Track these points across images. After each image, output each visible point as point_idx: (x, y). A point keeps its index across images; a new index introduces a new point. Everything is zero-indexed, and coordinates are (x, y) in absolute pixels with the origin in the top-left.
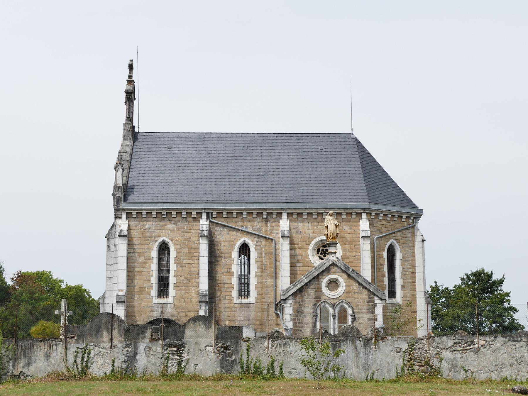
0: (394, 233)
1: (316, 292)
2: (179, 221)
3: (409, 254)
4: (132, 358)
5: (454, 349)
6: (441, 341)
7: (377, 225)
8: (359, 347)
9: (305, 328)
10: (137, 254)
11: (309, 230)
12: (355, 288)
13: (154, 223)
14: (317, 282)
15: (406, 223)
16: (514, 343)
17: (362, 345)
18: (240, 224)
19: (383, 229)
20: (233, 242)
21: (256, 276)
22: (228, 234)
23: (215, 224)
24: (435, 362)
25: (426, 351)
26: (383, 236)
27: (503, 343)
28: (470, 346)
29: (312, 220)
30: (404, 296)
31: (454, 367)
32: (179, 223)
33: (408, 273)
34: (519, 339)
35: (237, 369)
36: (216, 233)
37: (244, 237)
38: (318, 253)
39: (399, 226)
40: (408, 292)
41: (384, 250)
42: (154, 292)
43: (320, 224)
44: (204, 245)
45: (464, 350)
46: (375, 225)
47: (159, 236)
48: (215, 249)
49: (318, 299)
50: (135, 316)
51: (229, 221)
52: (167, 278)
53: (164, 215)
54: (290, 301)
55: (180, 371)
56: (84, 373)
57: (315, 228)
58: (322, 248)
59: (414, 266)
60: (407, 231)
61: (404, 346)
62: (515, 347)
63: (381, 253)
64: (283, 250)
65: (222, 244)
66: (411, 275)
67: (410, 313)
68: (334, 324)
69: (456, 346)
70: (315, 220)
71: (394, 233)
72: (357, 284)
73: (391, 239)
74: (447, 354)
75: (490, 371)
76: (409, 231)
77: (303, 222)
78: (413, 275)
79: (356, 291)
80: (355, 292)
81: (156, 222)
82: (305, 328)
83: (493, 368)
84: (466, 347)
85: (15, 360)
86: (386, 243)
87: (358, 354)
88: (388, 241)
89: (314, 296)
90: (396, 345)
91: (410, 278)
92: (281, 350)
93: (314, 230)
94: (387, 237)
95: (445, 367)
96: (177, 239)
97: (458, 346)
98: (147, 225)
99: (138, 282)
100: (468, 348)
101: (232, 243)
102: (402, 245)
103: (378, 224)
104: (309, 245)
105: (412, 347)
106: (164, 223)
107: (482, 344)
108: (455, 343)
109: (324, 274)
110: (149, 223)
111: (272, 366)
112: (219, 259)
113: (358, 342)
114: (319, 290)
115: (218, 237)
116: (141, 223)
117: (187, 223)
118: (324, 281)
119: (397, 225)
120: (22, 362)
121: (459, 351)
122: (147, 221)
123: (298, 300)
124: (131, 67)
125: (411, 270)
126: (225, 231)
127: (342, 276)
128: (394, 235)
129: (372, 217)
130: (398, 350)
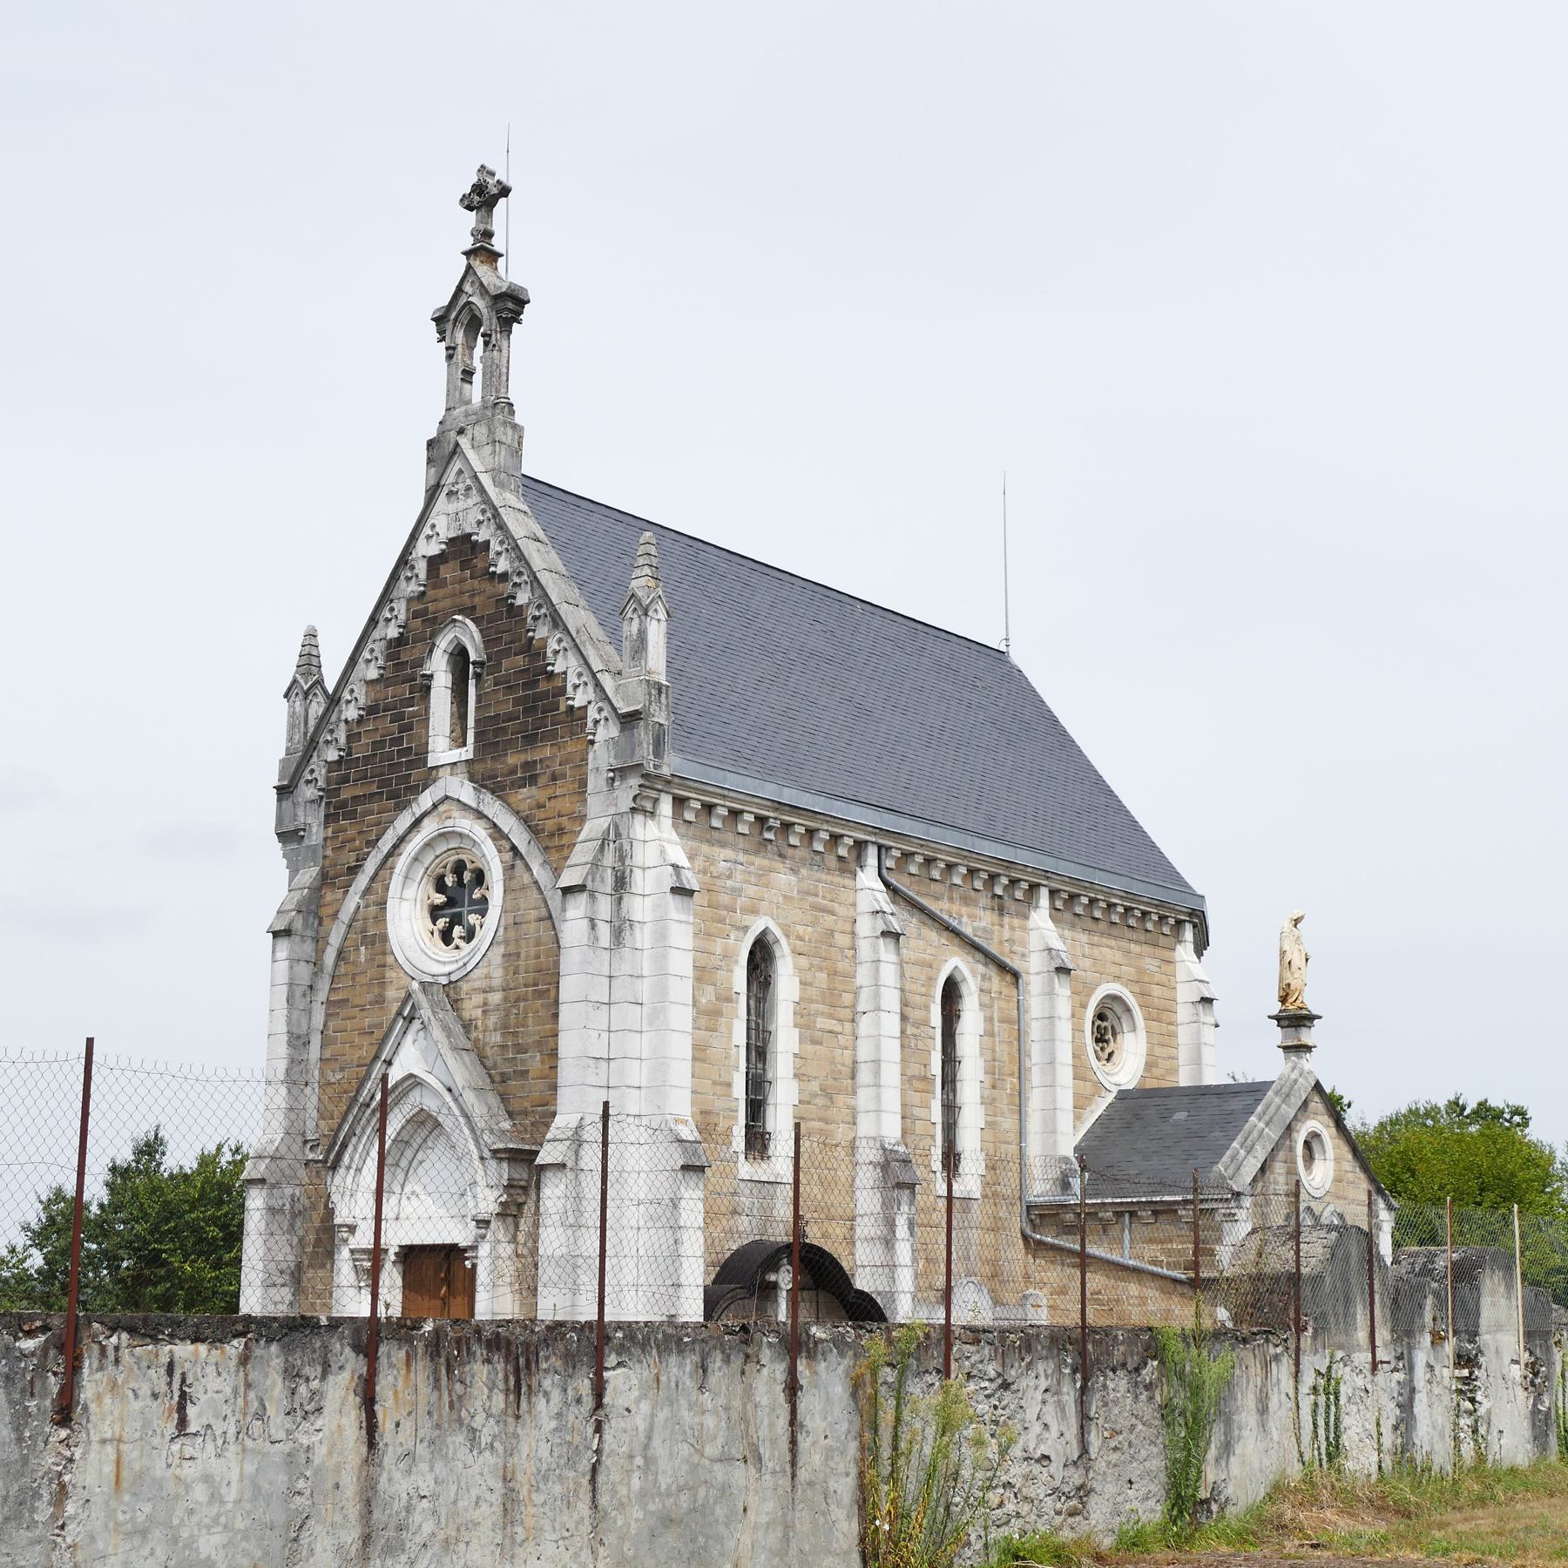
2: (803, 861)
13: (741, 857)
32: (804, 872)
43: (1104, 940)
47: (754, 911)
81: (746, 852)
96: (801, 929)
106: (766, 862)
117: (824, 876)
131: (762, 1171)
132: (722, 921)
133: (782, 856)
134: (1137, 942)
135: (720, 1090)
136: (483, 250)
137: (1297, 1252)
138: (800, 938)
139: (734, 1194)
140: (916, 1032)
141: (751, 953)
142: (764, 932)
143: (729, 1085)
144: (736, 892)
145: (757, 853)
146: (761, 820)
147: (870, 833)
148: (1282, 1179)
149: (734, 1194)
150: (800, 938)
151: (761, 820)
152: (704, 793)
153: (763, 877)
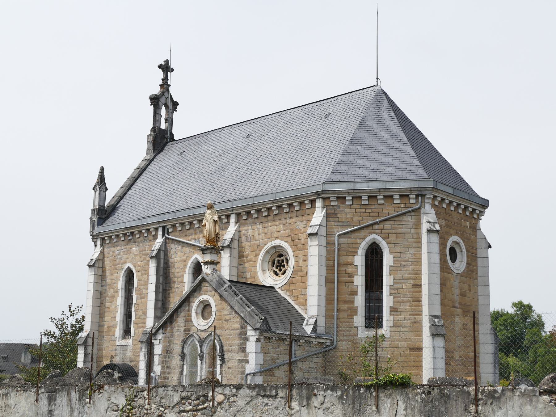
0: (376, 223)
1: (186, 321)
2: (141, 241)
3: (410, 255)
5: (182, 409)
6: (166, 394)
7: (344, 215)
8: (74, 400)
9: (173, 375)
10: (108, 286)
11: (259, 234)
12: (226, 313)
13: (123, 248)
14: (187, 308)
15: (402, 206)
16: (266, 400)
17: (78, 398)
18: (193, 237)
19: (354, 219)
20: (185, 261)
21: (297, 304)
22: (182, 251)
23: (171, 241)
25: (147, 410)
26: (352, 231)
27: (248, 399)
28: (204, 403)
29: (263, 219)
30: (396, 325)
32: (141, 245)
33: (406, 287)
34: (274, 393)
36: (172, 252)
37: (196, 253)
38: (273, 266)
40: (404, 317)
41: (356, 252)
42: (359, 320)
43: (271, 224)
46: (339, 215)
47: (125, 263)
48: (169, 273)
49: (187, 330)
50: (102, 361)
51: (184, 234)
52: (131, 313)
53: (129, 236)
54: (160, 337)
57: (266, 230)
58: (277, 259)
59: (418, 275)
60: (405, 218)
62: (266, 408)
63: (350, 258)
64: (223, 266)
65: (176, 265)
66: (412, 290)
67: (408, 352)
68: (202, 368)
69: (184, 404)
70: (266, 220)
71: (376, 223)
72: (229, 308)
73: (370, 233)
76: (409, 218)
77: (254, 223)
78: (416, 289)
79: (227, 317)
80: (226, 320)
81: (124, 245)
82: (173, 375)
84: (198, 405)
86: (359, 241)
87: (72, 411)
88: (364, 238)
89: (183, 328)
90: (113, 400)
91: (409, 295)
93: (265, 234)
94: (363, 232)
96: (139, 263)
97: (187, 404)
98: (117, 250)
100: (201, 407)
102: (394, 241)
103: (346, 212)
104: (258, 255)
106: (130, 246)
107: (220, 401)
108: (183, 398)
109: (196, 294)
110: (119, 248)
112: (173, 285)
113: (73, 393)
114: (189, 320)
115: (173, 257)
116: (113, 249)
117: (148, 244)
119: (385, 210)
121: (188, 411)
122: (117, 246)
123: (168, 334)
124: (166, 68)
125: (411, 282)
127: (213, 296)
128: (376, 227)
129: (333, 204)
130: (115, 408)
131: (124, 342)
132: (116, 269)
133: (135, 242)
134: (290, 218)
135: (113, 319)
136: (165, 85)
137: (377, 355)
138: (139, 266)
139: (115, 350)
140: (178, 286)
141: (133, 274)
142: (129, 268)
143: (115, 317)
144: (121, 258)
145: (127, 244)
146: (125, 235)
147: (158, 224)
148: (182, 325)
149: (115, 350)
150: (139, 266)
151: (125, 235)
152: (116, 232)
153: (129, 252)
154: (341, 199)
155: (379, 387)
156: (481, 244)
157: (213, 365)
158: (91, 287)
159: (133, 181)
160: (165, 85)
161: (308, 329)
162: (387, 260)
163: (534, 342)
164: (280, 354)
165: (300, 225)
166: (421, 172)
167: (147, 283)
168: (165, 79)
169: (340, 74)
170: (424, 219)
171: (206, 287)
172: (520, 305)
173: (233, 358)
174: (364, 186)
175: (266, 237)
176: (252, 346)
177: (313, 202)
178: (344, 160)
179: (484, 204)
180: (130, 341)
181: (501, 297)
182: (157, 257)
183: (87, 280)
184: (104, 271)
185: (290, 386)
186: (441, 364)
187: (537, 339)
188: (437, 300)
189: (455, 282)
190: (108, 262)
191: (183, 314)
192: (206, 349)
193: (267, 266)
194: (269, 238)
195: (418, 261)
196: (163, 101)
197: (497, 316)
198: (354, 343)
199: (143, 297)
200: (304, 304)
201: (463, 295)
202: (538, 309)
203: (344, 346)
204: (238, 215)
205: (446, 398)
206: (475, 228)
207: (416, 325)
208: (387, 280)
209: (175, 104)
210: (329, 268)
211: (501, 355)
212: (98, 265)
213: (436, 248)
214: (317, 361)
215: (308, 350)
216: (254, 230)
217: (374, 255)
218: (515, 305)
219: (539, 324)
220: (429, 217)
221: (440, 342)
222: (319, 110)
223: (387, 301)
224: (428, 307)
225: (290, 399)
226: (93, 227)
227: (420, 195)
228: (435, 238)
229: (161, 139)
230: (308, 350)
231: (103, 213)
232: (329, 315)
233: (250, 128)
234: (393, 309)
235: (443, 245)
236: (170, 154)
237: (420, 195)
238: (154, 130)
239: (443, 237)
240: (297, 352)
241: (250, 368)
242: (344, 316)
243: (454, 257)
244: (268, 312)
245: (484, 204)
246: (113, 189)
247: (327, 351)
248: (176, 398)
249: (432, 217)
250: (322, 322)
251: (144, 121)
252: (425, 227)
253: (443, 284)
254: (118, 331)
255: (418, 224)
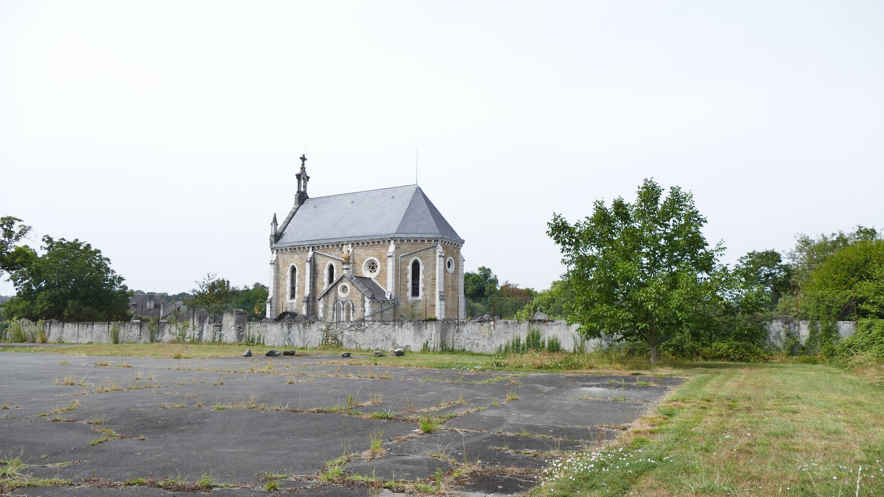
4: (201, 333)
24: (340, 338)
30: (425, 295)
31: (349, 341)
35: (244, 340)
39: (422, 247)
40: (428, 292)
42: (409, 293)
44: (308, 266)
45: (357, 330)
49: (336, 298)
55: (220, 340)
56: (199, 340)
59: (434, 274)
61: (324, 327)
74: (346, 333)
75: (370, 344)
83: (372, 342)
85: (158, 333)
92: (263, 329)
95: (345, 341)
98: (286, 256)
99: (281, 290)
101: (325, 264)
103: (404, 247)
105: (328, 328)
111: (259, 338)
114: (336, 293)
118: (340, 286)
120: (161, 334)
124: (303, 159)
126: (321, 257)
136: (303, 168)
154: (402, 241)
155: (427, 321)
156: (461, 259)
157: (348, 312)
158: (273, 274)
159: (290, 219)
160: (303, 168)
161: (388, 297)
162: (422, 268)
163: (491, 293)
164: (377, 307)
165: (383, 251)
166: (436, 230)
167: (304, 273)
168: (303, 165)
169: (401, 176)
170: (438, 251)
171: (344, 279)
172: (482, 269)
173: (359, 310)
174: (412, 235)
175: (365, 256)
176: (367, 305)
177: (389, 241)
178: (403, 223)
179: (463, 242)
180: (295, 301)
181: (471, 266)
182: (310, 261)
183: (270, 271)
184: (278, 266)
185: (395, 321)
186: (443, 311)
187: (493, 292)
188: (442, 285)
189: (449, 277)
190: (280, 261)
191: (698, 376)
192: (345, 306)
193: (367, 268)
194: (368, 255)
195: (435, 271)
196: (302, 177)
197: (468, 276)
198: (407, 303)
199: (303, 280)
200: (385, 286)
201: (453, 282)
202: (494, 273)
203: (402, 305)
204: (353, 244)
205: (448, 324)
206: (458, 253)
207: (433, 295)
208: (421, 276)
209: (308, 178)
210: (397, 271)
211: (470, 301)
212: (275, 264)
213: (442, 263)
214: (392, 310)
215: (388, 306)
216: (360, 252)
217: (416, 265)
218: (480, 269)
219: (495, 281)
220: (440, 249)
221: (443, 303)
222: (389, 193)
223: (421, 285)
224: (439, 288)
225: (395, 325)
226: (271, 243)
227: (436, 240)
228: (442, 259)
229: (302, 197)
230: (388, 306)
231: (277, 237)
232: (396, 291)
233: (353, 197)
234: (424, 289)
235: (445, 261)
236: (306, 205)
237: (436, 240)
238: (298, 192)
239: (445, 258)
240: (384, 307)
241: (367, 313)
242: (403, 291)
243: (449, 267)
244: (374, 292)
245: (463, 242)
246: (281, 222)
247: (395, 306)
248: (348, 326)
249: (441, 250)
250: (393, 295)
251: (293, 187)
252: (438, 254)
253: (445, 278)
254: (288, 296)
255: (435, 253)
